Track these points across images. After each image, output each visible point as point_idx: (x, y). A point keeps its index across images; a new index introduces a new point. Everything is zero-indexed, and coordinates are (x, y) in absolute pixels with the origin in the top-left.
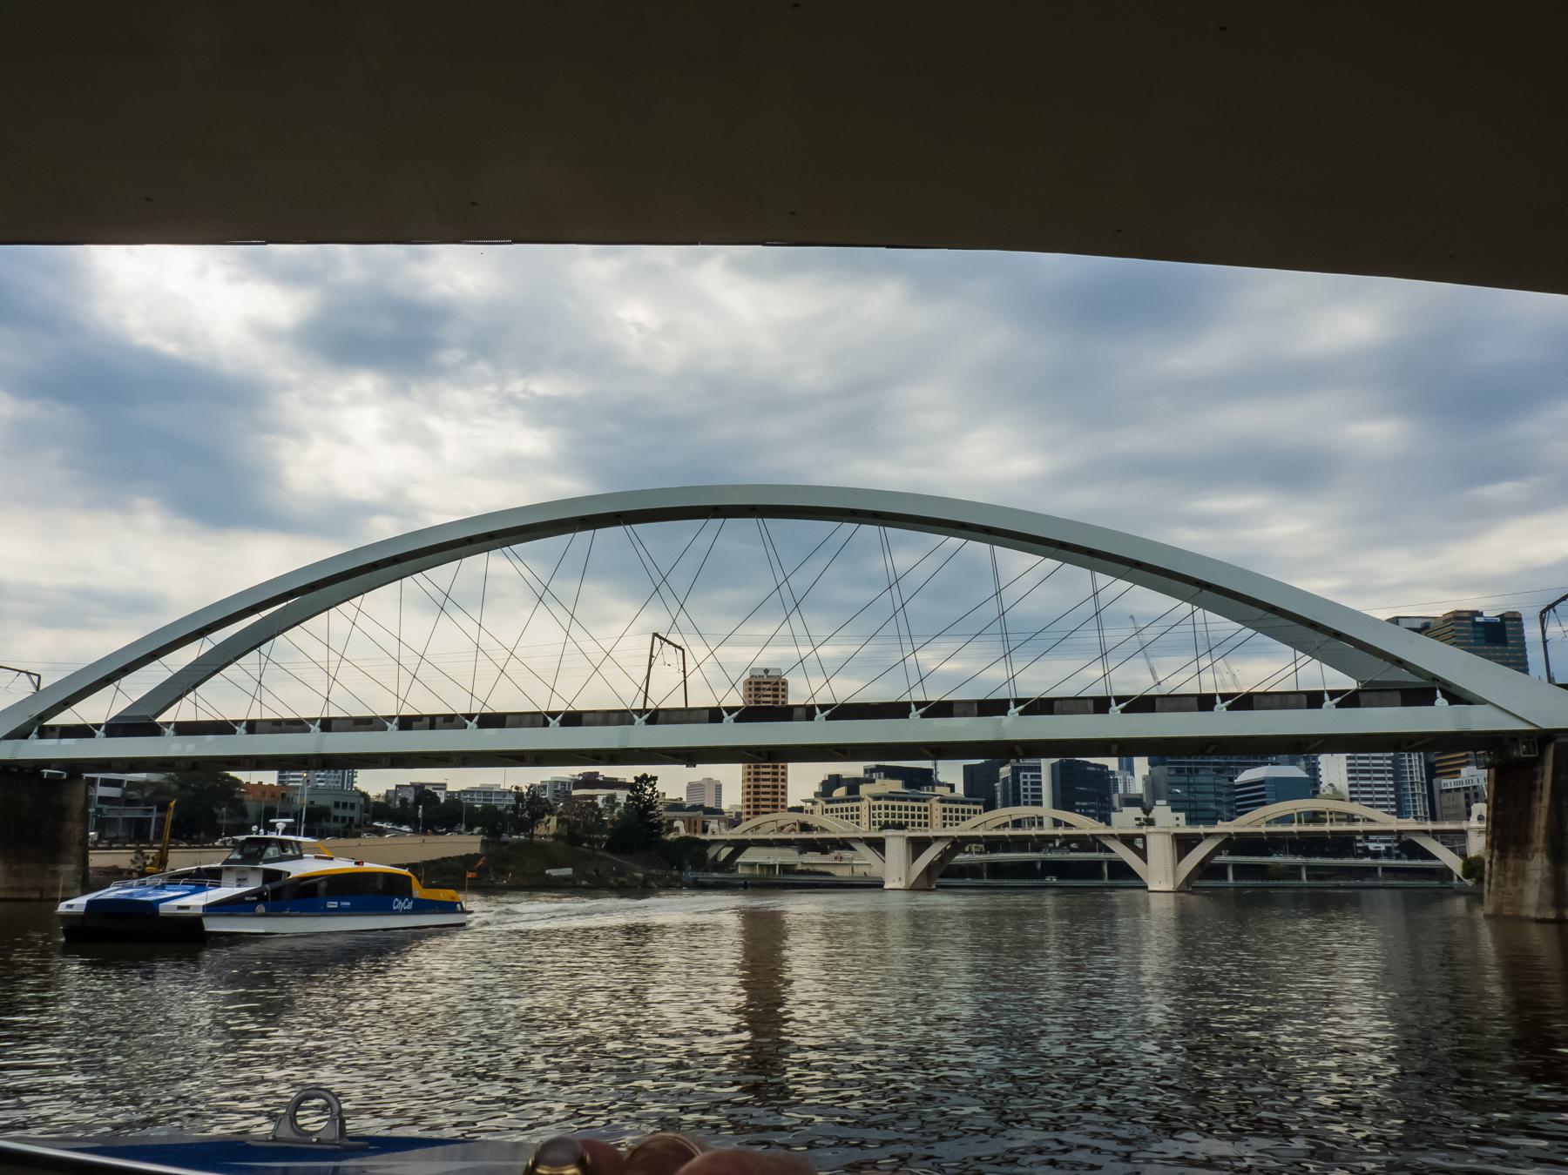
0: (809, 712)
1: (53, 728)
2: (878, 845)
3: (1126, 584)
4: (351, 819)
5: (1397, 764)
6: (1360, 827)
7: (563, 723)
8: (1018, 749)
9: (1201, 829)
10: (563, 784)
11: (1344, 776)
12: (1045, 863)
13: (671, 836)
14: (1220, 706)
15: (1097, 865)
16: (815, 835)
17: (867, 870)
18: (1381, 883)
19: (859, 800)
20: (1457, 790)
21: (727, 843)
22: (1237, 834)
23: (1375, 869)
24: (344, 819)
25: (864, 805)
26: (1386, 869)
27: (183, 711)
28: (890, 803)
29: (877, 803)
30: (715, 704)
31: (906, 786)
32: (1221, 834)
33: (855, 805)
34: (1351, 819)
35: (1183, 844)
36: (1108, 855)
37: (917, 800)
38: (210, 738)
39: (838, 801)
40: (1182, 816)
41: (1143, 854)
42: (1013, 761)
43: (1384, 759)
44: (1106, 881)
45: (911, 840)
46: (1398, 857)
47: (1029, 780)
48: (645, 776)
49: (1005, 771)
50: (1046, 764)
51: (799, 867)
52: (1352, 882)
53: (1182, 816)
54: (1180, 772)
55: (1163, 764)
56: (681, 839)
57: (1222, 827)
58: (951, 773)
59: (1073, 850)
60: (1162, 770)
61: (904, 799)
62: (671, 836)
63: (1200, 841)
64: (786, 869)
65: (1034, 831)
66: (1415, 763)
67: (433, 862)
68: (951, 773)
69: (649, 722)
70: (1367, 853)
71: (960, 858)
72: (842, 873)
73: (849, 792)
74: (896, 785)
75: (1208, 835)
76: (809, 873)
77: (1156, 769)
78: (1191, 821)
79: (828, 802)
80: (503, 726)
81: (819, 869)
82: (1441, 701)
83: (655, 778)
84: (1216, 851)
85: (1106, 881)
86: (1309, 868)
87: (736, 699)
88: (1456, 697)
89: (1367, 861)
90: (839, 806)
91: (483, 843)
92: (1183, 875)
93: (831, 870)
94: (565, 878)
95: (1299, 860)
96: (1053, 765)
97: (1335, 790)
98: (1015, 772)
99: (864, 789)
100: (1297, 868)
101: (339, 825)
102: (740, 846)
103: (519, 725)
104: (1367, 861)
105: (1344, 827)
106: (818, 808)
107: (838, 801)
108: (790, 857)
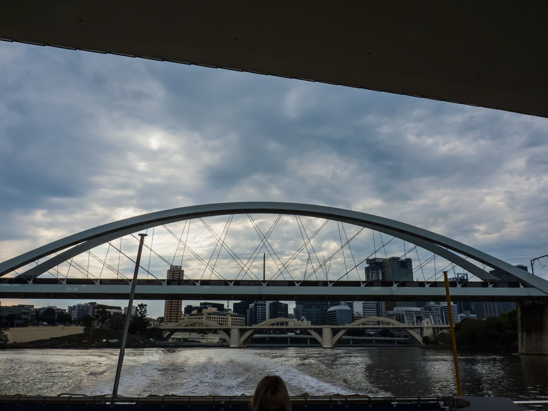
0: (421, 284)
1: (5, 279)
2: (320, 332)
3: (391, 237)
4: (27, 319)
5: (378, 305)
6: (391, 326)
7: (234, 284)
8: (232, 297)
9: (248, 327)
10: (82, 306)
11: (362, 309)
12: (270, 338)
13: (148, 327)
14: (427, 286)
15: (306, 339)
16: (209, 328)
17: (211, 340)
18: (375, 345)
19: (202, 315)
20: (393, 315)
21: (169, 330)
22: (258, 329)
23: (394, 341)
24: (24, 319)
25: (204, 317)
26: (376, 340)
27: (45, 275)
28: (214, 316)
29: (209, 316)
30: (325, 279)
31: (218, 310)
32: (254, 329)
33: (201, 316)
34: (388, 324)
35: (242, 332)
36: (309, 336)
37: (223, 315)
38: (84, 286)
39: (194, 315)
40: (310, 322)
41: (229, 335)
42: (255, 301)
43: (373, 304)
44: (289, 345)
45: (332, 329)
46: (377, 336)
47: (260, 309)
48: (142, 304)
49: (251, 305)
50: (268, 303)
51: (190, 339)
52: (380, 345)
53: (310, 322)
54: (306, 307)
55: (301, 304)
56: (153, 328)
57: (255, 326)
58: (292, 306)
59: (277, 334)
60: (300, 306)
61: (219, 315)
62: (148, 327)
63: (247, 331)
64: (185, 340)
65: (284, 327)
66: (383, 304)
67: (66, 337)
68: (229, 305)
69: (268, 285)
70: (370, 335)
71: (256, 336)
72: (204, 341)
73: (198, 312)
74: (215, 310)
75: (343, 328)
76: (193, 341)
77: (298, 306)
78: (312, 324)
79: (190, 315)
80: (317, 286)
81: (196, 340)
82: (521, 286)
83: (146, 305)
84: (344, 335)
85: (289, 345)
86: (353, 340)
87: (164, 276)
88: (526, 285)
89: (369, 338)
90: (195, 317)
91: (85, 329)
92: (334, 342)
93: (201, 341)
94: (116, 343)
95: (350, 337)
96: (270, 304)
97: (359, 314)
98: (256, 306)
99: (204, 311)
100: (349, 340)
101: (22, 322)
102: (173, 331)
103: (215, 285)
104: (369, 338)
105: (386, 326)
106: (186, 317)
107: (194, 315)
108: (186, 335)
